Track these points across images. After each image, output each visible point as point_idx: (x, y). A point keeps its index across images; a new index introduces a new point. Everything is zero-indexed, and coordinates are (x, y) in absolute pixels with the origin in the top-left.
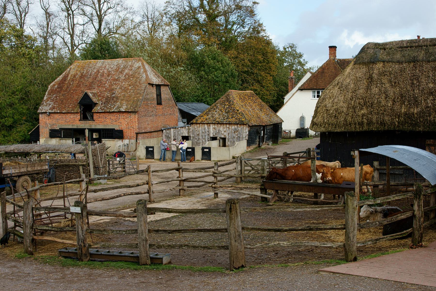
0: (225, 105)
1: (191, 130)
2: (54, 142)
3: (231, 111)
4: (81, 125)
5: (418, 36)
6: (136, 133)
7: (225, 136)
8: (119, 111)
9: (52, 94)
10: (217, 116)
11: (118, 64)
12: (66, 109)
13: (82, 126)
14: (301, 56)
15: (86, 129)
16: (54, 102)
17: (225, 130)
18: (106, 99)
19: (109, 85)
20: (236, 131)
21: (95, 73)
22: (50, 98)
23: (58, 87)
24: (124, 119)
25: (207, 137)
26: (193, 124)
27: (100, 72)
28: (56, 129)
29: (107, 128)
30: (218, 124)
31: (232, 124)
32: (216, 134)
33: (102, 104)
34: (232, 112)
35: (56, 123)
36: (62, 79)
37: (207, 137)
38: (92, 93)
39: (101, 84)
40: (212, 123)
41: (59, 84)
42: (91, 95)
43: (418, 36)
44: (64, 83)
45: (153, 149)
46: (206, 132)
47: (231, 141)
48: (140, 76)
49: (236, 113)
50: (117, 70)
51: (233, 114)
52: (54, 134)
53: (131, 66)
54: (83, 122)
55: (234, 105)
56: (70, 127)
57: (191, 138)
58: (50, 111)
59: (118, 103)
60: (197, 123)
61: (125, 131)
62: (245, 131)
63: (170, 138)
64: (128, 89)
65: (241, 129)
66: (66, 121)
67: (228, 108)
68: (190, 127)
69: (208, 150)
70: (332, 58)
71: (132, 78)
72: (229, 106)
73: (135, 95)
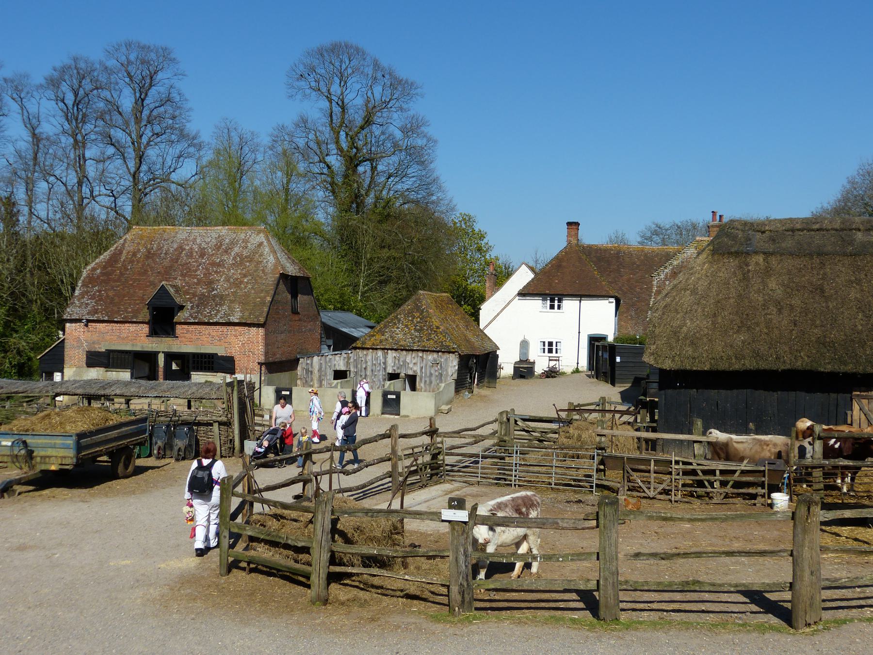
0: (414, 317)
1: (352, 360)
2: (95, 373)
3: (425, 328)
4: (150, 345)
5: (713, 212)
6: (259, 363)
7: (414, 371)
8: (228, 321)
9: (90, 286)
10: (400, 336)
11: (219, 236)
12: (121, 315)
13: (152, 347)
14: (482, 237)
15: (159, 352)
16: (97, 301)
17: (414, 361)
18: (200, 299)
19: (205, 274)
20: (436, 363)
21: (175, 250)
22: (87, 292)
23: (102, 274)
24: (235, 336)
25: (381, 373)
26: (355, 348)
27: (185, 249)
28: (100, 350)
29: (202, 351)
30: (402, 350)
31: (427, 351)
32: (398, 368)
33: (192, 307)
34: (427, 330)
35: (98, 340)
36: (110, 258)
37: (381, 373)
38: (173, 286)
39: (188, 271)
40: (392, 349)
41: (105, 267)
42: (172, 291)
43: (713, 212)
44: (114, 267)
45: (291, 393)
46: (380, 364)
47: (425, 382)
48: (264, 259)
49: (435, 331)
50: (218, 247)
51: (430, 334)
52: (94, 359)
53: (246, 241)
54: (155, 339)
55: (431, 318)
56: (128, 348)
57: (352, 375)
58: (88, 317)
59: (225, 307)
60: (363, 349)
61: (237, 359)
62: (452, 364)
63: (312, 372)
64: (241, 282)
65: (446, 360)
66: (119, 337)
67: (420, 322)
68: (351, 355)
69: (394, 397)
70: (574, 242)
71: (250, 262)
72: (421, 319)
73: (255, 293)
